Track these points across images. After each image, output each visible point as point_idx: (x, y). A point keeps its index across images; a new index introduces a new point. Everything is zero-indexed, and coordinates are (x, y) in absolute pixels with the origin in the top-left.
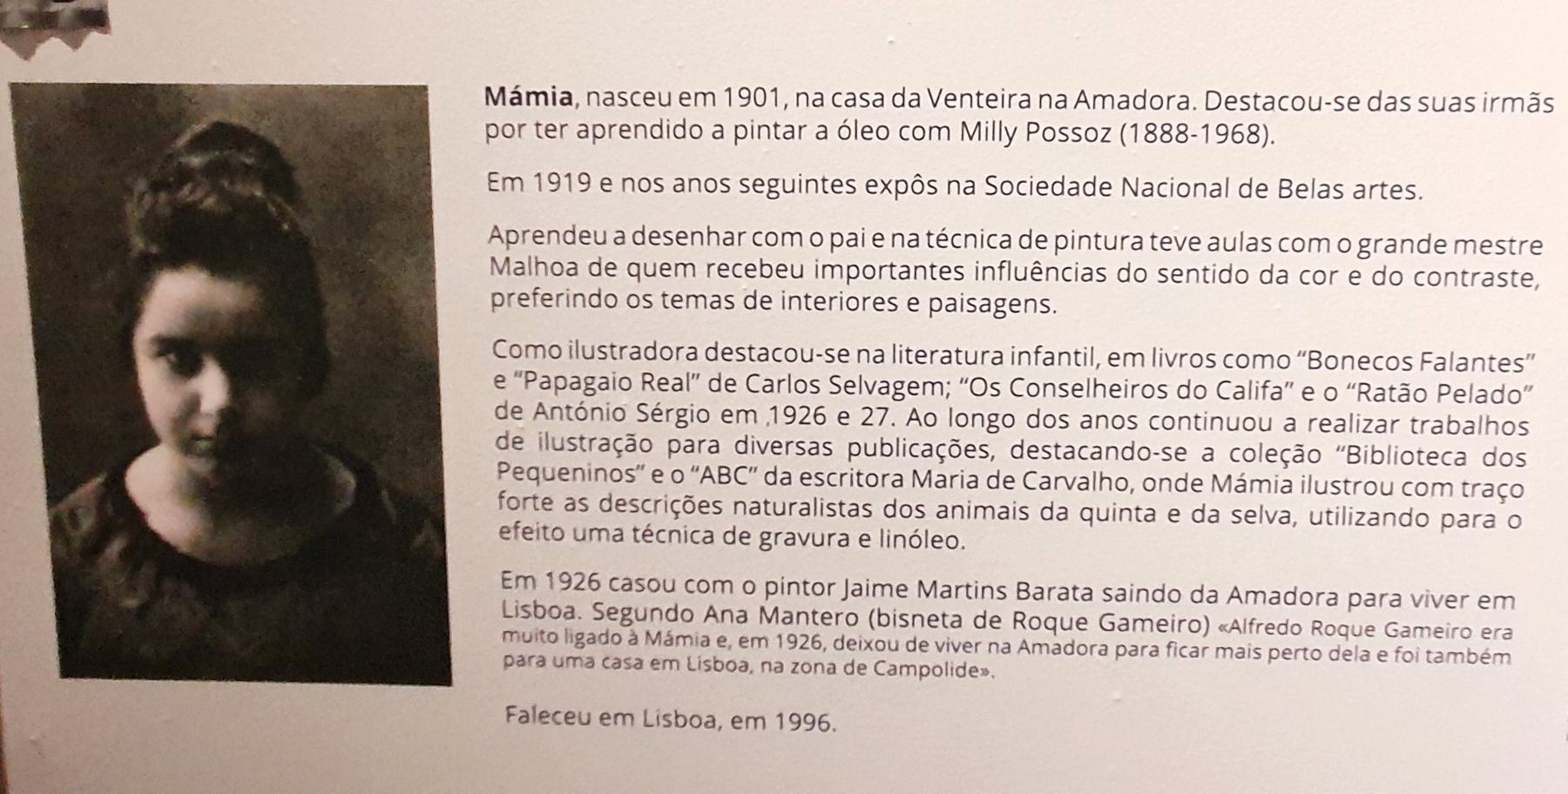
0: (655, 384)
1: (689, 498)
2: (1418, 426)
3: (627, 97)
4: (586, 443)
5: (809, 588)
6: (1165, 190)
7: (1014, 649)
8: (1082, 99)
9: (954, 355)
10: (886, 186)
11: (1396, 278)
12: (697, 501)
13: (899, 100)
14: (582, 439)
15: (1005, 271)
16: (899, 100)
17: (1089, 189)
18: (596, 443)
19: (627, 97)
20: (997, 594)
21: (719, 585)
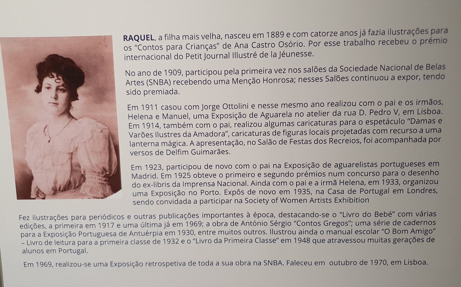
0: (333, 141)
2: (346, 43)
3: (237, 36)
5: (312, 223)
10: (404, 78)
12: (420, 30)
13: (185, 135)
15: (180, 152)
16: (185, 135)
19: (237, 36)
21: (404, 231)
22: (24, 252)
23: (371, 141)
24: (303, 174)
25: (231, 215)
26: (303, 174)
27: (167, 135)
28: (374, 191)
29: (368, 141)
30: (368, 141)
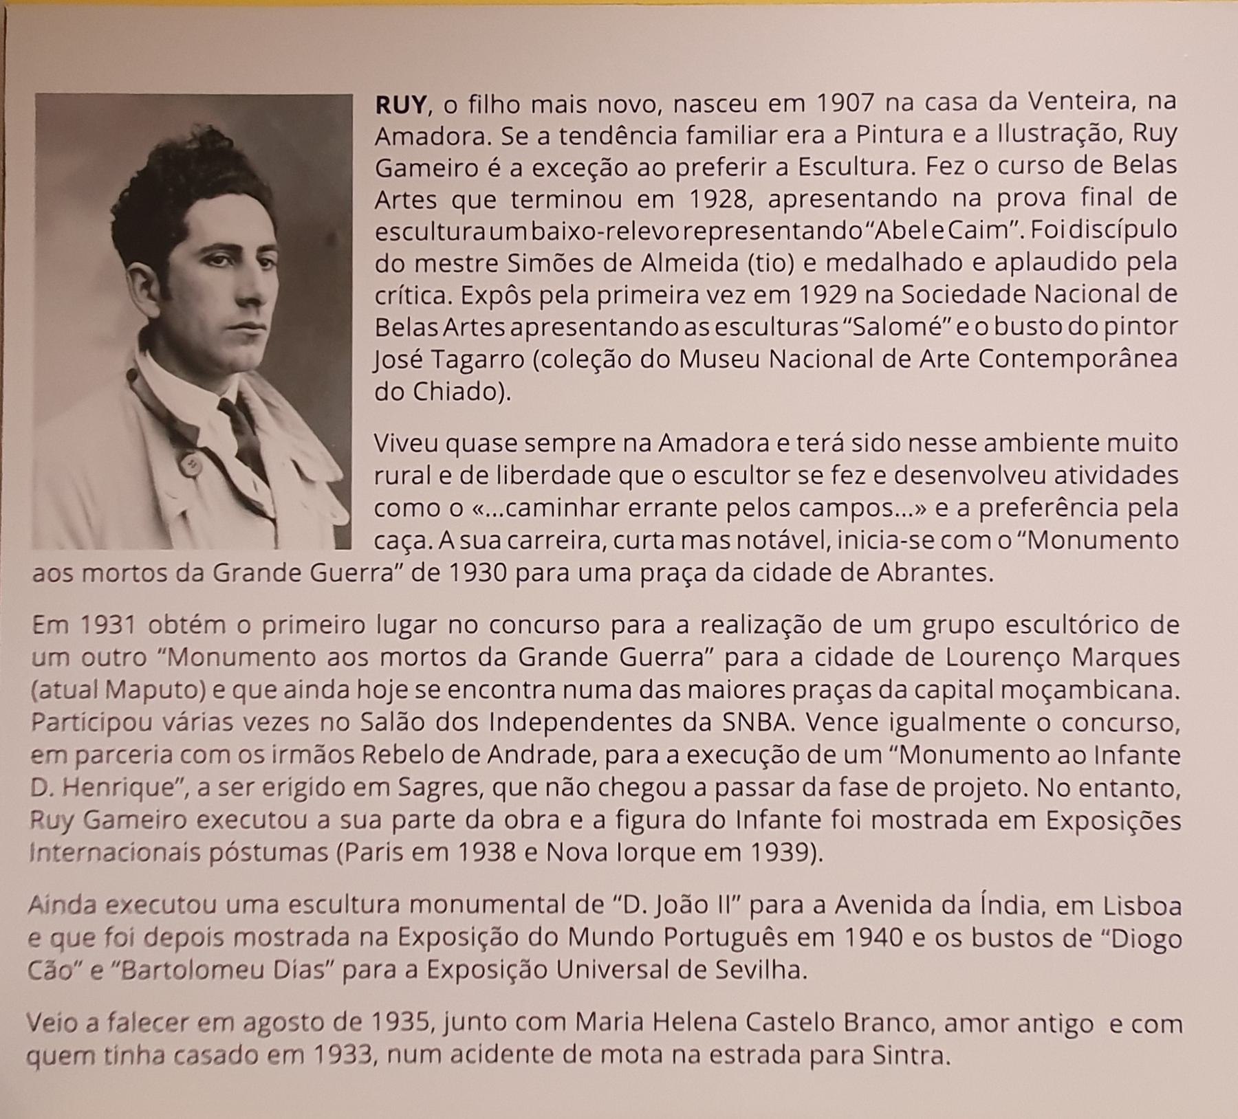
0: (376, 756)
1: (560, 256)
4: (294, 938)
6: (1077, 296)
7: (655, 445)
8: (666, 442)
9: (1068, 475)
11: (398, 393)
14: (289, 933)
17: (1143, 477)
18: (304, 938)
20: (470, 540)
22: (40, 576)
23: (856, 822)
24: (1052, 509)
25: (790, 820)
26: (1052, 509)
27: (922, 820)
28: (784, 327)
29: (847, 821)
30: (847, 821)
